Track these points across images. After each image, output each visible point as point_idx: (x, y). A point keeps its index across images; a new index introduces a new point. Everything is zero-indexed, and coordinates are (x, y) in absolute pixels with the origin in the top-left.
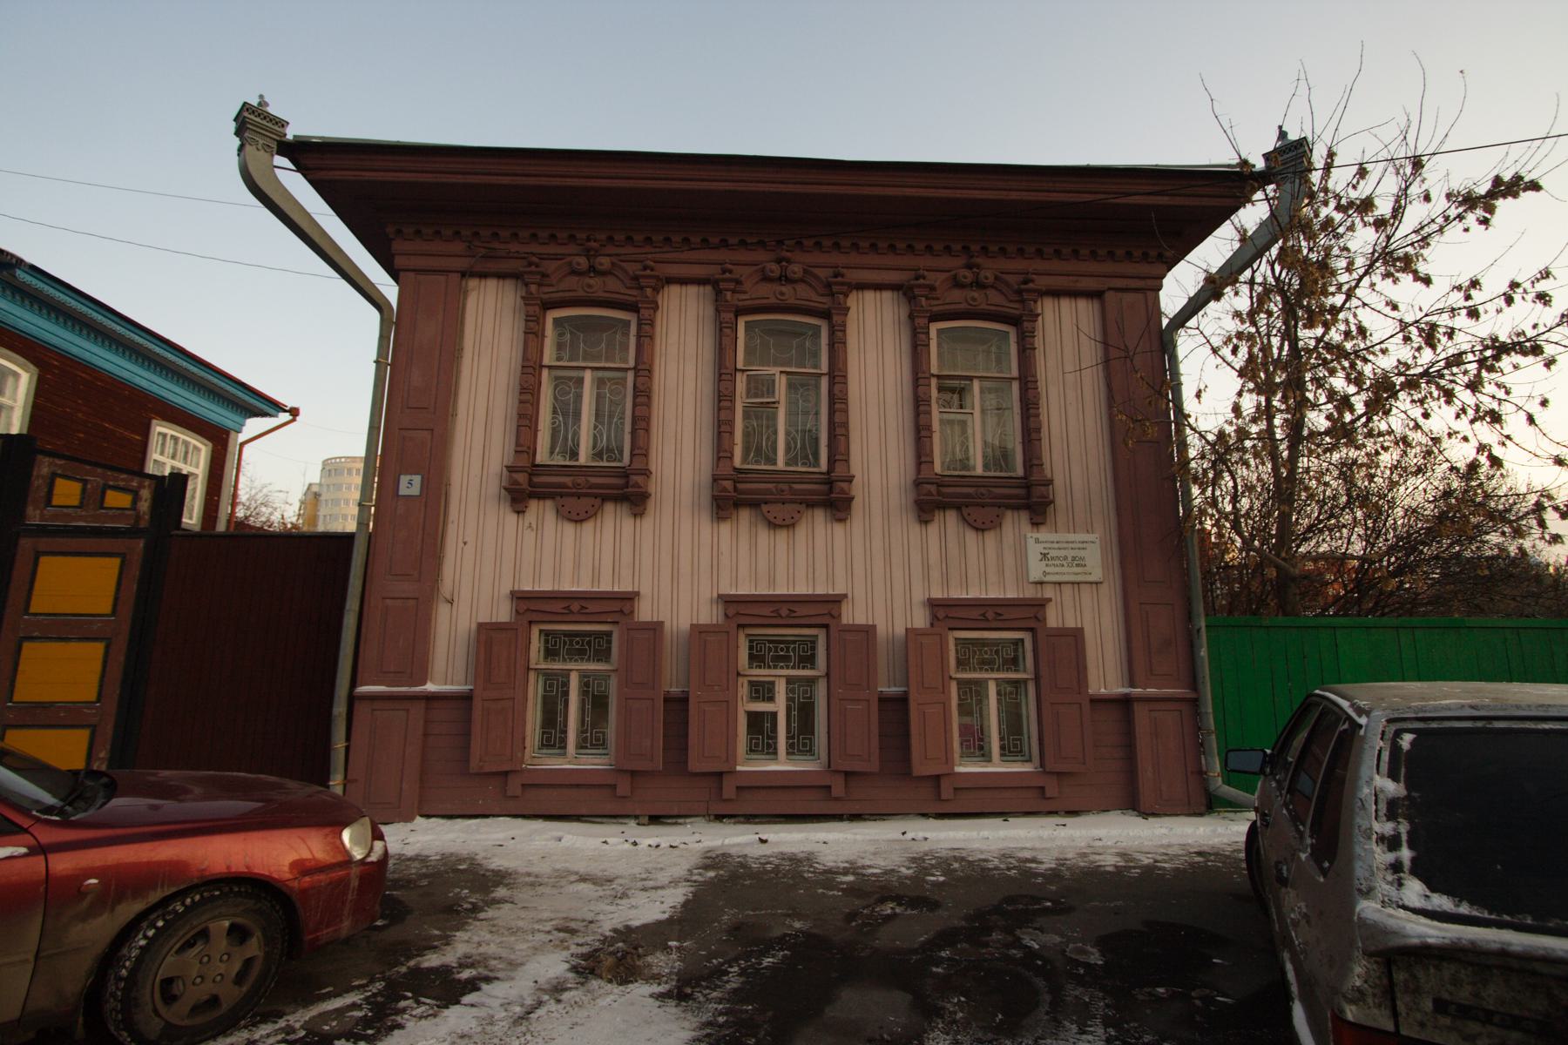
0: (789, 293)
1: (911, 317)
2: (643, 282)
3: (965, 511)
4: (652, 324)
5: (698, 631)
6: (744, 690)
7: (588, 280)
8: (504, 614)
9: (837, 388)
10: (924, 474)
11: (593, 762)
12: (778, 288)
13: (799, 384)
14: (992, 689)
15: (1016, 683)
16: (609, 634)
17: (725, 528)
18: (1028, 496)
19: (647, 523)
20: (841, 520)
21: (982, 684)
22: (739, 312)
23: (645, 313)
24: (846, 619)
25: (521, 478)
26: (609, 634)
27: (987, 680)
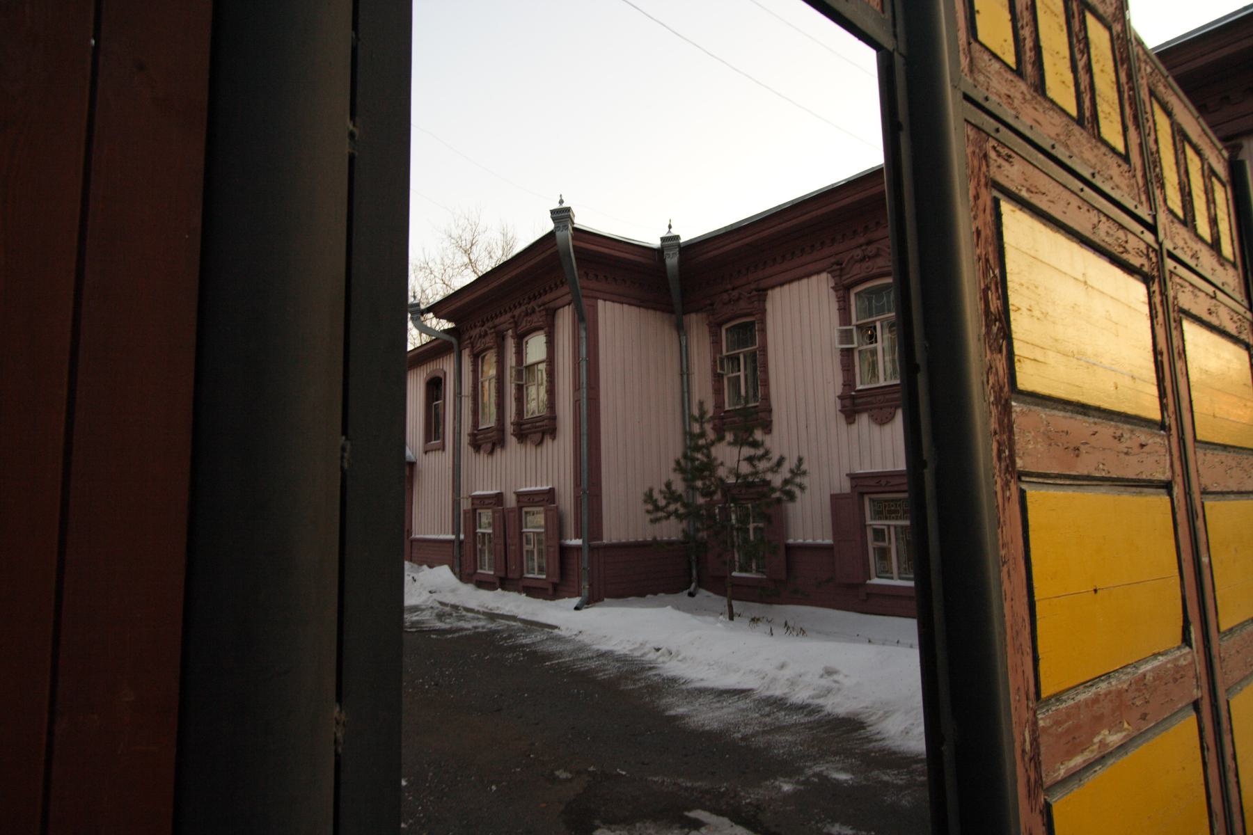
8: (846, 487)
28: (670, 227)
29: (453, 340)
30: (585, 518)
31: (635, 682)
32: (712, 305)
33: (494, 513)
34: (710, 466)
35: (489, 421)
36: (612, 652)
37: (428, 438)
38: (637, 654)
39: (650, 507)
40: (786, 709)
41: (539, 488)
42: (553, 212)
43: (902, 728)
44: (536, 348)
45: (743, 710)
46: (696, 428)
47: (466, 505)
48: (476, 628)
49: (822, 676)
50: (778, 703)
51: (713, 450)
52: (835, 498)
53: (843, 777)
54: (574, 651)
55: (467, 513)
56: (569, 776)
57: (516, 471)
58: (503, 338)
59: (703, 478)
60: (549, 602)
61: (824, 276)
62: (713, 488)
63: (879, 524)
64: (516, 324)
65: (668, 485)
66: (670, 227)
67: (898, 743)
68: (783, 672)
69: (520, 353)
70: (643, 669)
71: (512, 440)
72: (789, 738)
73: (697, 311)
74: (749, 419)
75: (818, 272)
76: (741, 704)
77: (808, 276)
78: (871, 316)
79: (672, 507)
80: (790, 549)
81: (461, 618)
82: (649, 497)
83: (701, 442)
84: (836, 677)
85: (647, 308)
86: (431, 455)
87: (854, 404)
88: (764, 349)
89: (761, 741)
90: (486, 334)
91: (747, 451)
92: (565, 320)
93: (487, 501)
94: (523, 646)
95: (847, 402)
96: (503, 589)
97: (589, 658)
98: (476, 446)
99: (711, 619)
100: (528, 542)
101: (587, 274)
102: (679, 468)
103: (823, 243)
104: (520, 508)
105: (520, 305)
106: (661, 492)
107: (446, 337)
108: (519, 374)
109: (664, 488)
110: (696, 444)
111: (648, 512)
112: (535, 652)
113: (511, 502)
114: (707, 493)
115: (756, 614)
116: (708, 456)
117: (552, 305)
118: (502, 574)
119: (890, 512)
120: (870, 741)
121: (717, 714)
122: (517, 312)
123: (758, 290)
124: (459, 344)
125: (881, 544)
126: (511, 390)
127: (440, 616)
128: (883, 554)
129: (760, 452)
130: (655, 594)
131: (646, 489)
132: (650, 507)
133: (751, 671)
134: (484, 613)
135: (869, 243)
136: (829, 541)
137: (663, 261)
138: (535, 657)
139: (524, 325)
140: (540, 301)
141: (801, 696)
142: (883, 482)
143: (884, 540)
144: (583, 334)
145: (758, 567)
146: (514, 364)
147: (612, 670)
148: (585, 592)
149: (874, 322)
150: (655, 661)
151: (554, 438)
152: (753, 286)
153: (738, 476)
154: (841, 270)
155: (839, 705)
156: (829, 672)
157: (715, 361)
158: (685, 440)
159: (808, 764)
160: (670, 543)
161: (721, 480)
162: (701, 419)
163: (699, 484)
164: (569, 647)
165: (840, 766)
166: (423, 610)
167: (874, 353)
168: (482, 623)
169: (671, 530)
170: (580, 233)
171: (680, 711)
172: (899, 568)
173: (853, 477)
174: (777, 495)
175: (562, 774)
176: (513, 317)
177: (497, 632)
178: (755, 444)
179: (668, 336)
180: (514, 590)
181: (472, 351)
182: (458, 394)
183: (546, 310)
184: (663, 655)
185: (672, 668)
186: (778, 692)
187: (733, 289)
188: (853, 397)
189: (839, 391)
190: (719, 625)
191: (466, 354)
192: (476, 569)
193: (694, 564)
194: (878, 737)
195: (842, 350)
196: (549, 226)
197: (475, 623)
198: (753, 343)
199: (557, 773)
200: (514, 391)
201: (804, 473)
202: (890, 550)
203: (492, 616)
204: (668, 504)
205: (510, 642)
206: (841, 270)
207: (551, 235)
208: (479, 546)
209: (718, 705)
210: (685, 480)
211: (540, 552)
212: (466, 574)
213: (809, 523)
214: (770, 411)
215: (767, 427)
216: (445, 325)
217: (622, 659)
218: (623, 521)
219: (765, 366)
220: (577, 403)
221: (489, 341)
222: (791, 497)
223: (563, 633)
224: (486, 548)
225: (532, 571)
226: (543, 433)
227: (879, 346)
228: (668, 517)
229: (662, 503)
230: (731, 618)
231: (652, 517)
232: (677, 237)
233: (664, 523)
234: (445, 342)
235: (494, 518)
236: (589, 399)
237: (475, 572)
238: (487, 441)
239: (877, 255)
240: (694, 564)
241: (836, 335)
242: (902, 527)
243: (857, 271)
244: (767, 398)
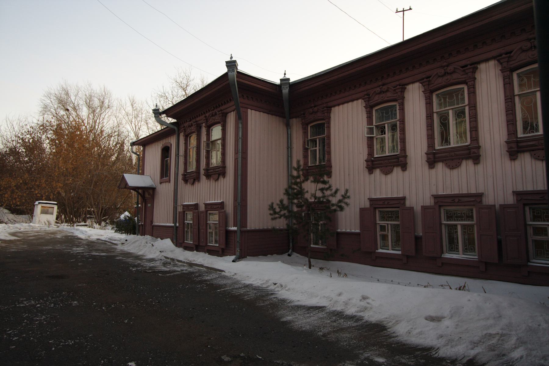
2: (467, 71)
4: (474, 87)
5: (424, 208)
6: (530, 231)
7: (382, 95)
8: (367, 205)
11: (473, 257)
12: (445, 78)
13: (460, 114)
17: (433, 171)
18: (470, 153)
19: (407, 173)
21: (456, 225)
22: (513, 70)
23: (470, 83)
25: (514, 145)
28: (285, 74)
29: (176, 128)
30: (239, 217)
31: (264, 301)
32: (304, 114)
33: (193, 213)
34: (301, 193)
35: (192, 168)
36: (251, 285)
37: (162, 176)
38: (264, 286)
39: (272, 212)
40: (344, 318)
41: (216, 202)
42: (227, 62)
43: (406, 330)
44: (216, 133)
45: (321, 318)
46: (295, 173)
47: (180, 209)
48: (182, 270)
49: (361, 300)
50: (339, 315)
51: (303, 184)
52: (362, 210)
53: (381, 360)
54: (232, 283)
55: (181, 212)
56: (230, 359)
57: (205, 193)
58: (200, 127)
59: (297, 199)
60: (221, 258)
61: (360, 101)
62: (303, 203)
63: (383, 223)
64: (207, 120)
65: (281, 201)
66: (285, 74)
67: (405, 338)
68: (340, 298)
69: (208, 135)
70: (268, 295)
71: (203, 178)
72: (348, 335)
73: (296, 117)
74: (322, 171)
75: (357, 99)
76: (321, 315)
77: (352, 101)
78: (382, 121)
79: (282, 213)
80: (339, 234)
81: (175, 265)
82: (271, 207)
83: (298, 180)
84: (368, 301)
85: (272, 115)
86: (163, 185)
88: (329, 137)
89: (332, 337)
90: (192, 125)
91: (321, 186)
92: (231, 118)
93: (190, 208)
94: (206, 281)
95: (370, 163)
96: (197, 251)
97: (240, 288)
98: (186, 180)
99: (300, 268)
100: (210, 228)
101: (243, 96)
102: (287, 193)
103: (355, 86)
104: (207, 211)
105: (209, 111)
106: (278, 205)
107: (172, 126)
108: (208, 145)
109: (279, 203)
110: (296, 181)
111: (271, 214)
112: (212, 284)
113: (202, 208)
114: (299, 206)
115: (321, 266)
116: (301, 188)
117: (225, 111)
118: (197, 243)
120: (391, 337)
121: (308, 320)
122: (207, 115)
123: (327, 107)
124: (179, 130)
126: (203, 153)
127: (165, 264)
128: (384, 237)
129: (327, 186)
130: (272, 254)
131: (270, 203)
132: (272, 212)
133: (324, 297)
134: (187, 263)
135: (383, 85)
136: (358, 231)
137: (281, 91)
138: (213, 287)
139: (211, 121)
140: (219, 109)
141: (351, 311)
142: (386, 203)
143: (385, 231)
144: (240, 126)
145: (322, 243)
146: (205, 140)
147: (252, 294)
148: (238, 253)
149: (384, 124)
150: (273, 290)
151: (224, 177)
152: (325, 105)
153: (315, 198)
154: (369, 98)
155: (371, 317)
156: (364, 298)
157: (304, 142)
158: (288, 179)
159: (360, 352)
160: (281, 230)
161: (307, 200)
162: (298, 169)
163: (295, 201)
164: (229, 282)
165: (377, 352)
166: (156, 261)
167: (383, 140)
168: (186, 268)
169: (281, 224)
170: (241, 75)
171: (289, 318)
172: (392, 245)
173: (371, 200)
174: (334, 207)
175: (226, 358)
176: (206, 117)
177: (193, 273)
178: (324, 182)
179: (282, 129)
180: (203, 251)
181: (185, 134)
182: (177, 155)
183: (222, 113)
184: (278, 287)
185: (283, 294)
186: (339, 308)
187: (315, 107)
188: (372, 161)
189: (366, 157)
190: (305, 271)
191: (182, 135)
192: (184, 240)
193: (291, 240)
194: (394, 335)
195: (368, 137)
196: (225, 70)
197: (182, 268)
198: (324, 133)
199: (223, 357)
200: (205, 154)
201: (349, 197)
202: (388, 236)
203: (191, 265)
204: (281, 211)
205: (199, 279)
206: (369, 98)
207: (226, 75)
208: (186, 229)
209: (308, 315)
210: (289, 199)
211: (216, 233)
212: (179, 243)
213: (348, 222)
214: (331, 167)
215: (329, 175)
216: (171, 120)
217: (257, 289)
218: (258, 218)
220: (236, 160)
221: (193, 128)
222: (342, 209)
223: (226, 274)
224: (189, 230)
225: (211, 242)
226: (219, 175)
227: (386, 136)
228: (280, 218)
229: (278, 210)
230: (310, 268)
231: (273, 217)
232: (289, 79)
233: (278, 220)
234: (172, 129)
235: (193, 216)
236: (242, 158)
237: (184, 242)
238: (191, 178)
239: (387, 91)
240: (291, 240)
241: (366, 130)
242: (394, 225)
243: (377, 98)
244: (329, 160)
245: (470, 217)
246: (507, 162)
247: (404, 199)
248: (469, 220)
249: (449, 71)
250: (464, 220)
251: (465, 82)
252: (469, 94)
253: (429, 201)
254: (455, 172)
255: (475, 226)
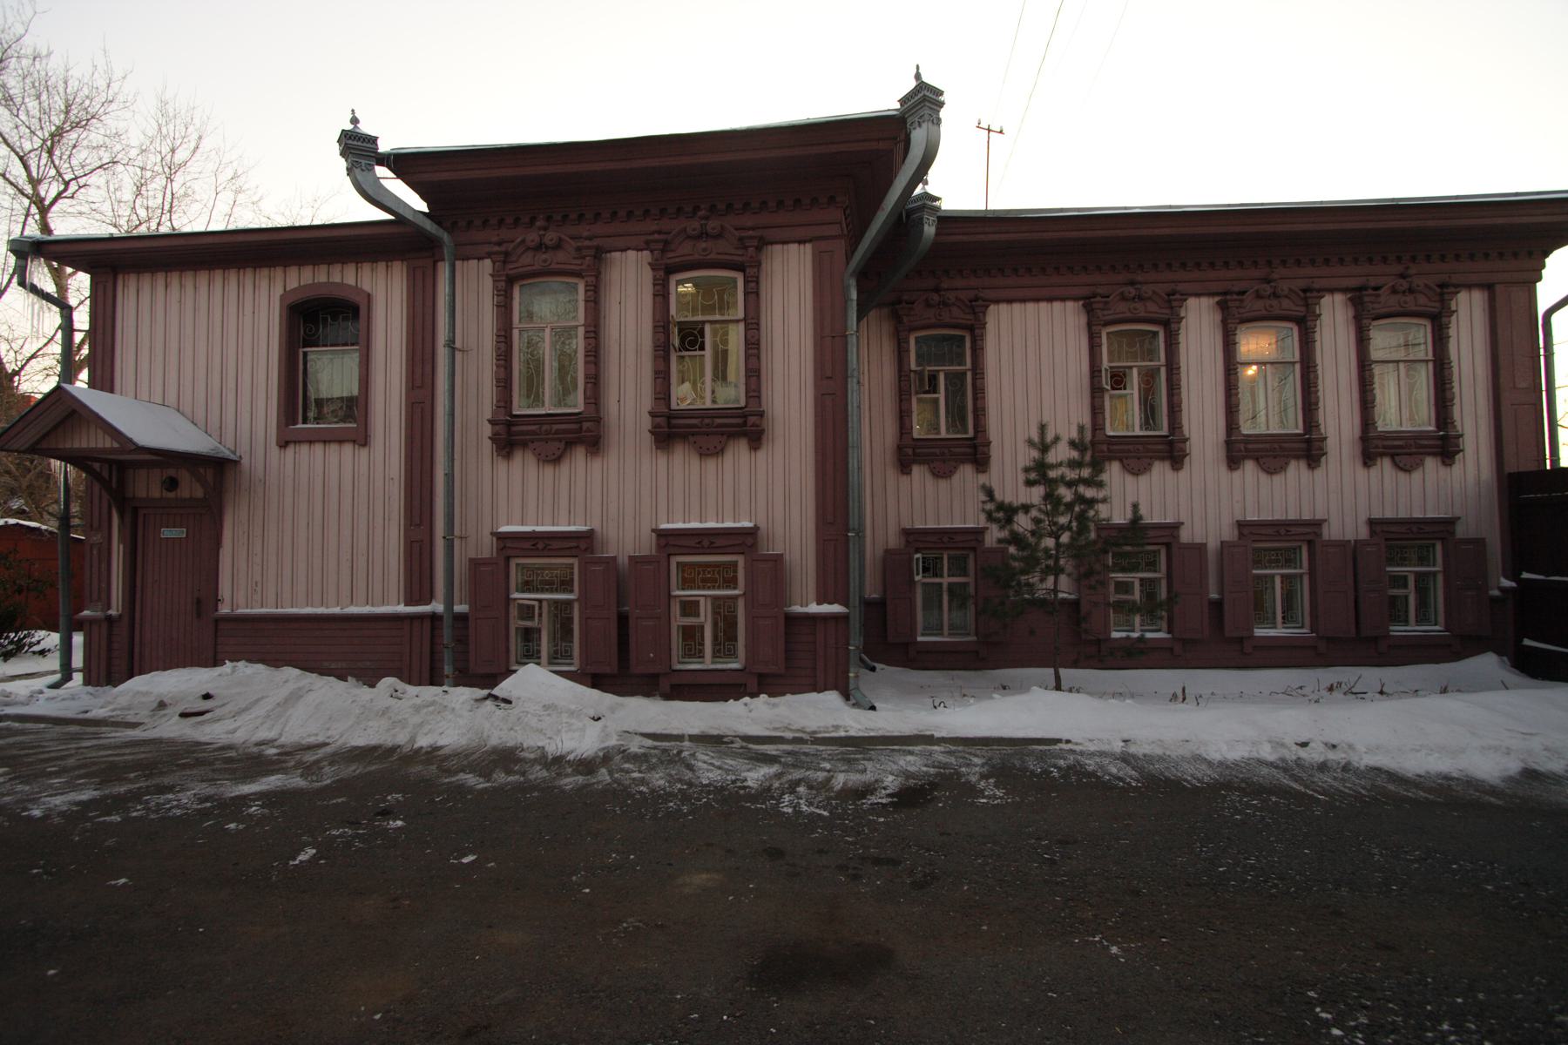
0: (1141, 309)
1: (1089, 325)
3: (1397, 459)
9: (502, 376)
10: (1099, 437)
11: (1436, 629)
14: (1278, 581)
15: (1151, 580)
16: (735, 564)
17: (1237, 475)
20: (984, 472)
24: (1326, 536)
26: (735, 564)
27: (1273, 576)
87: (509, 433)
88: (978, 371)
119: (704, 580)
125: (528, 624)
128: (529, 635)
143: (532, 618)
219: (979, 392)
239: (558, 246)
245: (566, 585)
246: (1361, 472)
247: (1176, 527)
248: (728, 587)
249: (709, 230)
250: (557, 591)
251: (740, 268)
252: (746, 294)
253: (647, 546)
254: (1277, 479)
255: (576, 606)
